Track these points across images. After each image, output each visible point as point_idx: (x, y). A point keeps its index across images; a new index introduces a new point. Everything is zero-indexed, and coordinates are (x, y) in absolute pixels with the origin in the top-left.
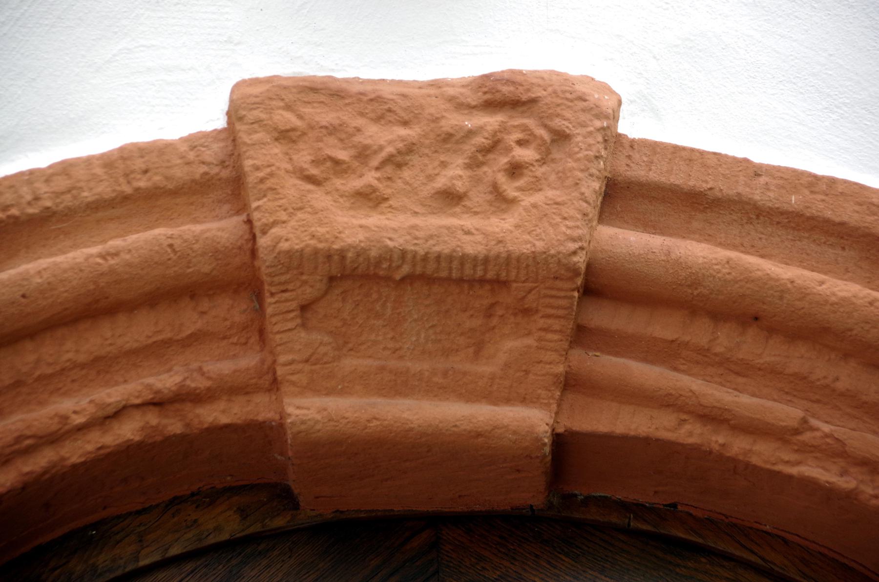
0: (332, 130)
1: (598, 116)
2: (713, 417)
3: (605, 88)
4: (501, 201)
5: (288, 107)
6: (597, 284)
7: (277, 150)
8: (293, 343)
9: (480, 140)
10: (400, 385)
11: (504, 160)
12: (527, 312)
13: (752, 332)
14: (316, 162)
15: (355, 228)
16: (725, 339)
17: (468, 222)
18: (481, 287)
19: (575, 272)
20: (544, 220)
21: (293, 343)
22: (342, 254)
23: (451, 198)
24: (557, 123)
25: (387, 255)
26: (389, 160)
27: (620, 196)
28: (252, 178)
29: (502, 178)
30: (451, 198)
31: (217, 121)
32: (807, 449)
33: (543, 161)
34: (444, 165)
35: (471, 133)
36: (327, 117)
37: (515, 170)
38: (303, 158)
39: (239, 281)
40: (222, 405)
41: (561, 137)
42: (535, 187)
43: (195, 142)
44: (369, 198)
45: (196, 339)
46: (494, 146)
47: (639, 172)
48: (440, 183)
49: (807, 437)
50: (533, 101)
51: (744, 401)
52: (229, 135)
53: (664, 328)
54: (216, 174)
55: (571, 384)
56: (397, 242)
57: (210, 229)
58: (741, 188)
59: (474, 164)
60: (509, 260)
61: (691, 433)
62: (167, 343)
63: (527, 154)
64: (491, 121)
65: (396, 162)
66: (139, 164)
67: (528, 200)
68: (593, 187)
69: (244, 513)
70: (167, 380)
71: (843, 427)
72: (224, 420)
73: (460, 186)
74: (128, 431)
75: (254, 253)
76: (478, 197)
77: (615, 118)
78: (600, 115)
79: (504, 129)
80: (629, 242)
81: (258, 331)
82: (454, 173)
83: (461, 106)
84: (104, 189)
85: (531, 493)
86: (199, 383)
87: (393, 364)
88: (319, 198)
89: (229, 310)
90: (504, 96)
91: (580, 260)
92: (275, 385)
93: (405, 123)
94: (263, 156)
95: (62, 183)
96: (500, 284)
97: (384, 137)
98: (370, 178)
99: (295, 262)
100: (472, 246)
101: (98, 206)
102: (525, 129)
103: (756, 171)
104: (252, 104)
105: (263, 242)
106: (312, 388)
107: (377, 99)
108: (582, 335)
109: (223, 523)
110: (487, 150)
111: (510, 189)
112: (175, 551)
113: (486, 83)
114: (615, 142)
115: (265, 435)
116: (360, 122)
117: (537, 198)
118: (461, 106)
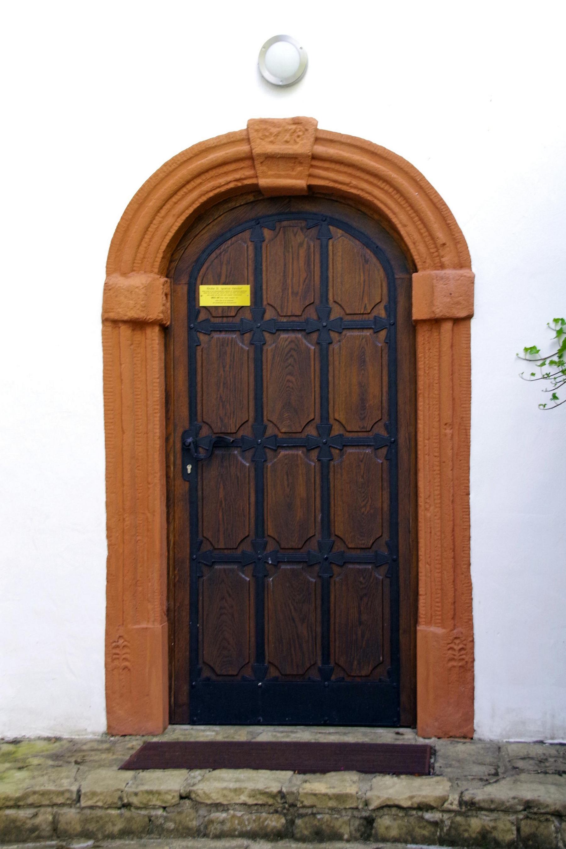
0: (265, 129)
1: (313, 126)
2: (335, 181)
3: (315, 120)
4: (296, 142)
5: (257, 125)
6: (314, 157)
7: (255, 133)
8: (260, 169)
9: (292, 131)
10: (279, 176)
11: (296, 135)
12: (301, 163)
13: (342, 165)
14: (263, 136)
15: (271, 148)
16: (337, 167)
17: (290, 147)
18: (293, 159)
19: (309, 156)
20: (302, 147)
21: (260, 169)
22: (267, 154)
23: (287, 142)
24: (306, 127)
25: (275, 154)
26: (275, 135)
27: (317, 140)
28: (251, 139)
29: (296, 138)
30: (287, 142)
31: (245, 127)
32: (351, 187)
33: (303, 134)
34: (286, 136)
35: (290, 130)
36: (264, 127)
37: (298, 136)
38: (260, 135)
39: (250, 158)
40: (248, 180)
41: (307, 130)
42: (302, 140)
43: (241, 131)
44: (272, 142)
45: (242, 168)
46: (295, 132)
47: (321, 135)
48: (285, 139)
49: (351, 185)
50: (301, 123)
51: (341, 178)
52: (247, 130)
53: (327, 165)
54: (245, 137)
55: (310, 175)
56: (277, 151)
57: (244, 148)
58: (339, 139)
59: (291, 135)
60: (297, 154)
61: (331, 184)
62: (238, 169)
63: (300, 133)
64: (294, 127)
65: (277, 135)
66: (231, 136)
67: (301, 142)
68: (312, 139)
69: (254, 196)
70: (237, 176)
71: (315, 472)
72: (248, 183)
73: (288, 140)
74: (232, 185)
75: (252, 153)
76: (292, 142)
77: (317, 125)
78: (313, 126)
79: (296, 128)
80: (320, 149)
81: (253, 167)
82: (287, 137)
83: (289, 124)
84: (225, 141)
85: (305, 193)
86: (243, 177)
87: (278, 173)
88: (263, 143)
89: (248, 163)
90: (297, 121)
91: (310, 154)
92: (257, 177)
93: (278, 127)
94: (253, 135)
95: (218, 140)
96: (296, 158)
97: (274, 130)
98: (272, 139)
99: (259, 155)
100: (291, 152)
101: (225, 144)
102: (300, 128)
103: (342, 135)
104: (252, 123)
105: (253, 151)
106: (264, 177)
107: (273, 123)
108: (312, 166)
109: (251, 198)
110: (294, 133)
111: (298, 140)
112: (242, 203)
113: (293, 119)
114: (317, 130)
115: (257, 185)
116: (270, 128)
117: (303, 142)
118: (289, 124)
